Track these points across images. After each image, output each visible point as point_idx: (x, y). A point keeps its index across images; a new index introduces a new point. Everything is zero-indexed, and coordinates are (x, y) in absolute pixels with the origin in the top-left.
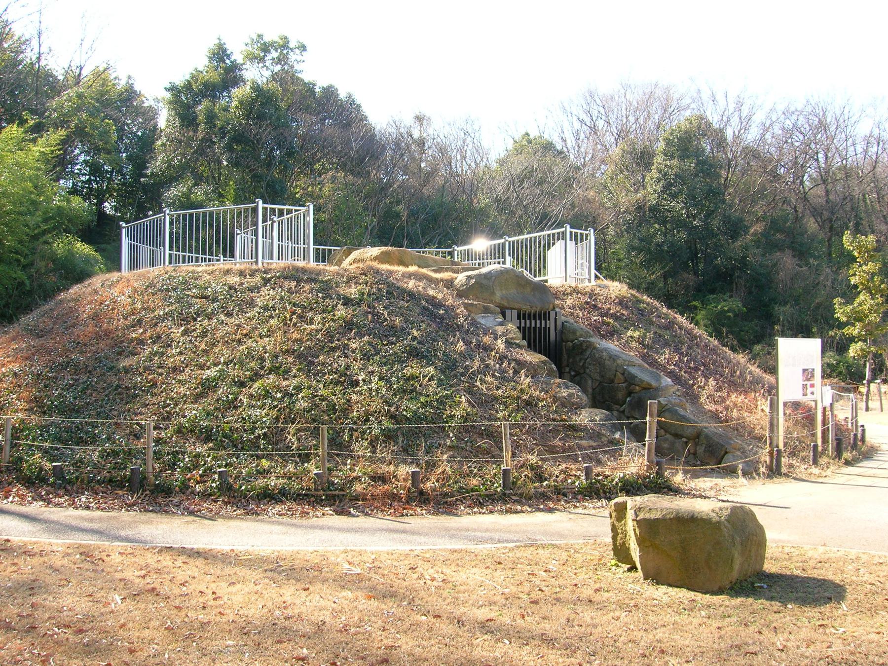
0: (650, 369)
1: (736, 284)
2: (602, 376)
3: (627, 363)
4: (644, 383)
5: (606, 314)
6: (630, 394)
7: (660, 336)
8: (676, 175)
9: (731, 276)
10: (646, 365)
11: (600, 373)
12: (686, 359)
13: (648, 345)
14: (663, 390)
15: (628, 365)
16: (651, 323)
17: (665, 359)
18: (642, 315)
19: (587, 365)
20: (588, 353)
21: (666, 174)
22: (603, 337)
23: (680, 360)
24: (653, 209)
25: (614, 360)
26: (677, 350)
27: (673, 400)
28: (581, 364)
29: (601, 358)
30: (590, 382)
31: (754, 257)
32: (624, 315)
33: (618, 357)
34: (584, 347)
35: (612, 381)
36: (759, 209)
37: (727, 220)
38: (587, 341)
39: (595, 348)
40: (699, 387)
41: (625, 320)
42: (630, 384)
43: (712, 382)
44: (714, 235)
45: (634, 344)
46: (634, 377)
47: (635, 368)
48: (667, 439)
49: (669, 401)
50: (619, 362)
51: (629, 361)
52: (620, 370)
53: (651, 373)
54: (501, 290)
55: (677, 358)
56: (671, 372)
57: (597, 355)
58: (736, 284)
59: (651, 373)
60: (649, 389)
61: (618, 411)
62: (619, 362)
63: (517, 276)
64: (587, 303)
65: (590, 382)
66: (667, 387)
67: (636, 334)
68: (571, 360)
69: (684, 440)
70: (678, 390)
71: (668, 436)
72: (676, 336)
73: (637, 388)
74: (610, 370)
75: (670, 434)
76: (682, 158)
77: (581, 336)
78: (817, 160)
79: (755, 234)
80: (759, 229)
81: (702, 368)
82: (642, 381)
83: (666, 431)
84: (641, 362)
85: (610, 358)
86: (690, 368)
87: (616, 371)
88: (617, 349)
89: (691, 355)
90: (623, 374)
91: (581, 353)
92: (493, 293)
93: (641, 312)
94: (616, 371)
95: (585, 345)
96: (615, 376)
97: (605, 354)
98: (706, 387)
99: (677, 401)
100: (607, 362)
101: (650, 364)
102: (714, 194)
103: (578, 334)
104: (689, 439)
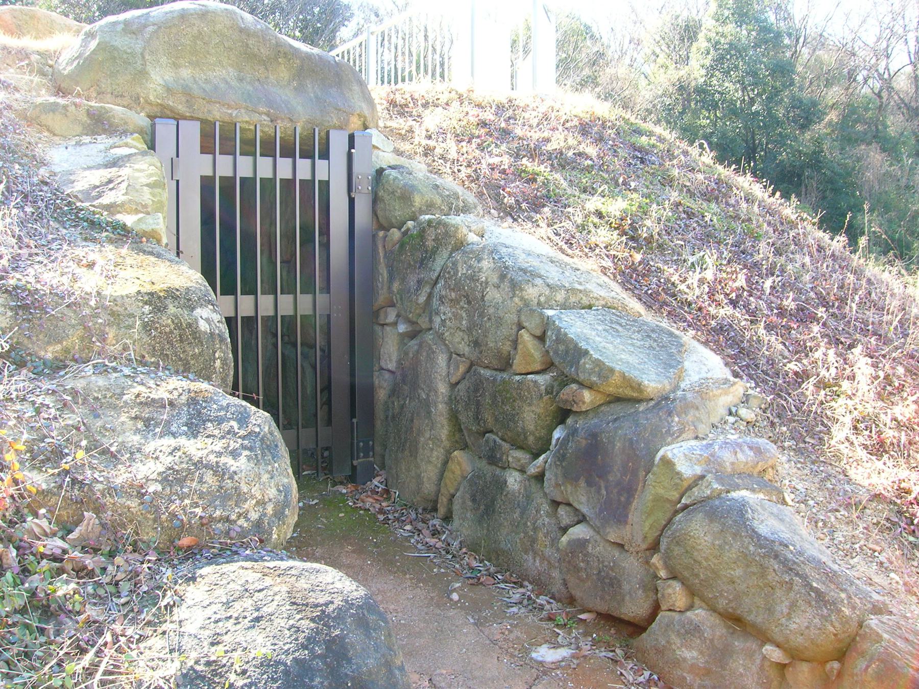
0: (648, 317)
1: (806, 187)
2: (476, 344)
3: (560, 296)
4: (615, 379)
5: (534, 153)
6: (563, 415)
7: (690, 215)
8: (731, 44)
9: (799, 176)
10: (636, 306)
11: (469, 330)
12: (768, 283)
13: (649, 240)
14: (687, 406)
15: (564, 306)
16: (668, 181)
17: (702, 281)
18: (642, 161)
19: (435, 302)
20: (439, 262)
21: (717, 43)
22: (510, 213)
23: (753, 287)
24: (700, 91)
25: (515, 286)
26: (740, 254)
27: (727, 456)
28: (422, 299)
29: (473, 278)
30: (441, 360)
31: (831, 152)
32: (588, 157)
33: (531, 274)
34: (430, 244)
35: (506, 364)
36: (834, 94)
37: (797, 103)
38: (440, 223)
39: (460, 245)
40: (822, 384)
41: (589, 169)
42: (565, 380)
43: (862, 366)
44: (779, 123)
45: (603, 236)
46: (576, 353)
47: (590, 315)
48: (694, 630)
49: (712, 462)
50: (532, 292)
51: (574, 291)
52: (532, 324)
53: (650, 333)
54: (176, 66)
55: (741, 281)
56: (720, 329)
57: (462, 270)
58: (806, 187)
59: (650, 333)
60: (639, 401)
61: (522, 471)
62: (532, 292)
63: (241, 30)
64: (483, 124)
65: (441, 360)
66: (703, 391)
67: (615, 207)
68: (396, 286)
69: (774, 653)
70: (746, 400)
71: (699, 614)
72: (737, 217)
73: (587, 395)
74: (499, 321)
75: (713, 609)
76: (740, 23)
77: (430, 207)
78: (906, 42)
79: (830, 123)
80: (834, 118)
81: (821, 312)
82: (604, 371)
83: (691, 592)
84: (616, 292)
85: (503, 277)
86: (782, 312)
87: (521, 327)
88: (546, 249)
89: (783, 271)
90: (541, 338)
91: (423, 263)
92: (142, 74)
93: (641, 155)
94: (521, 327)
95: (431, 235)
96: (515, 343)
97: (486, 264)
98: (846, 385)
99: (745, 457)
100: (493, 295)
101: (652, 301)
102: (783, 70)
103: (418, 201)
104: (795, 655)
